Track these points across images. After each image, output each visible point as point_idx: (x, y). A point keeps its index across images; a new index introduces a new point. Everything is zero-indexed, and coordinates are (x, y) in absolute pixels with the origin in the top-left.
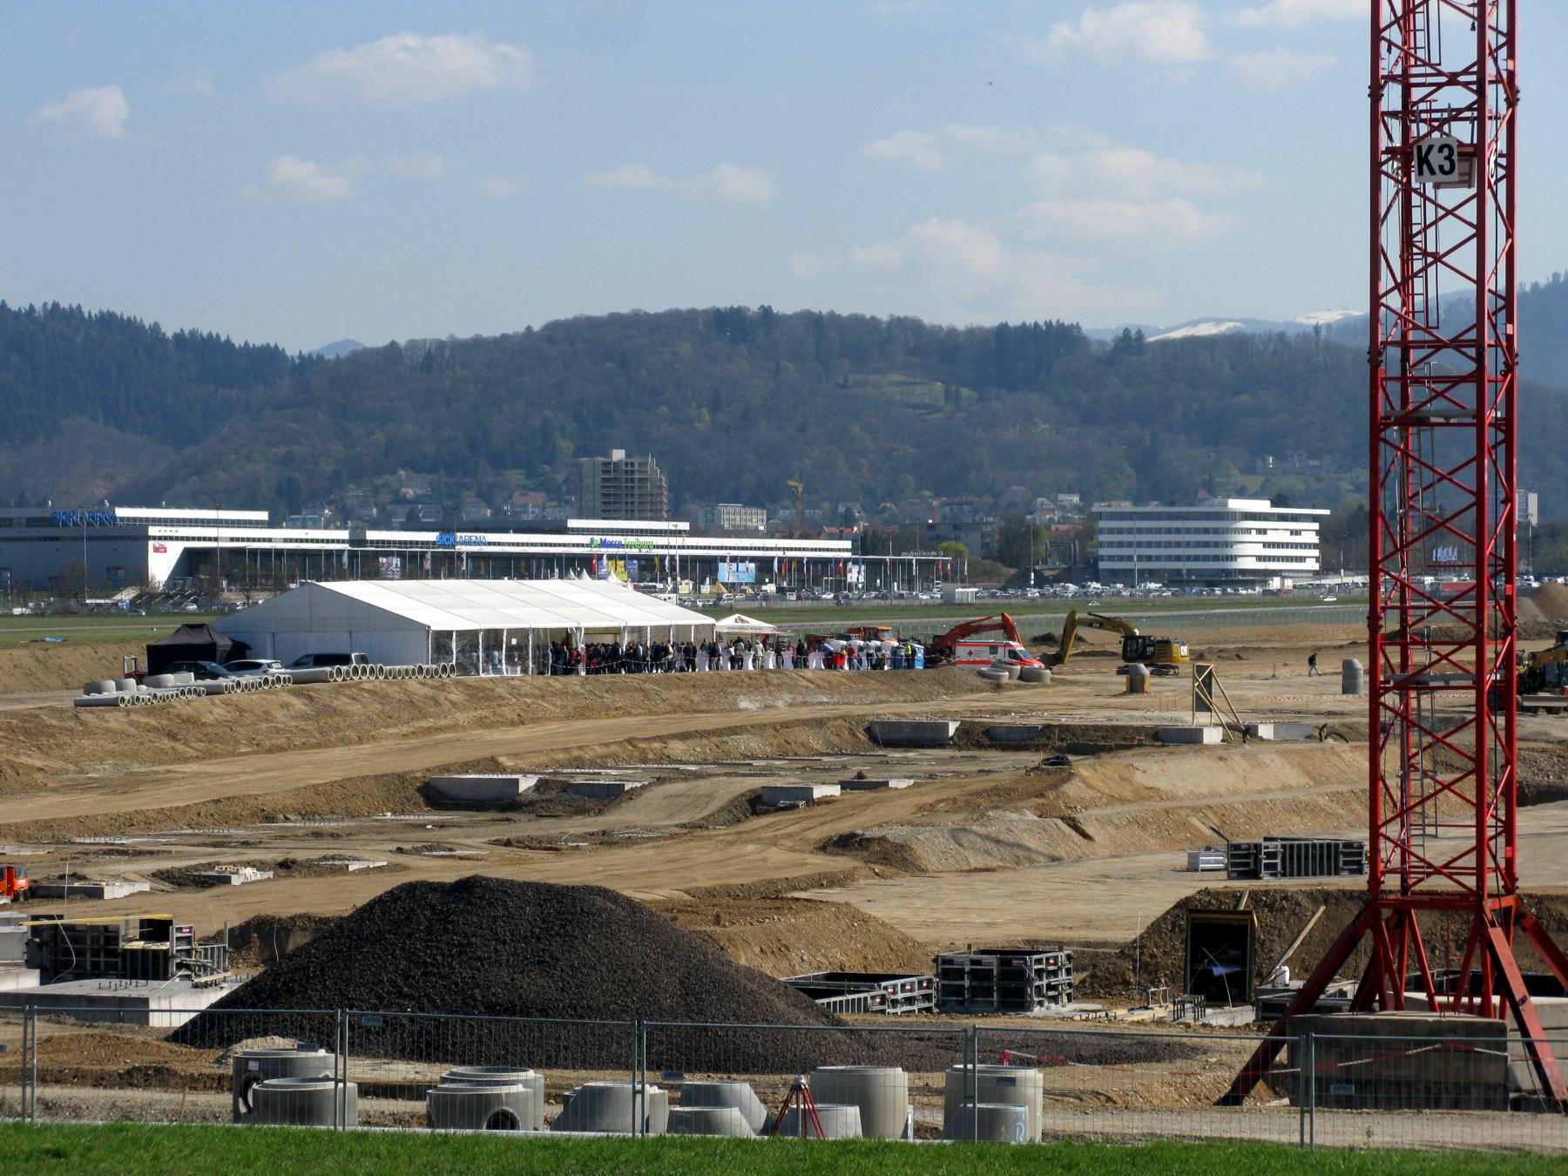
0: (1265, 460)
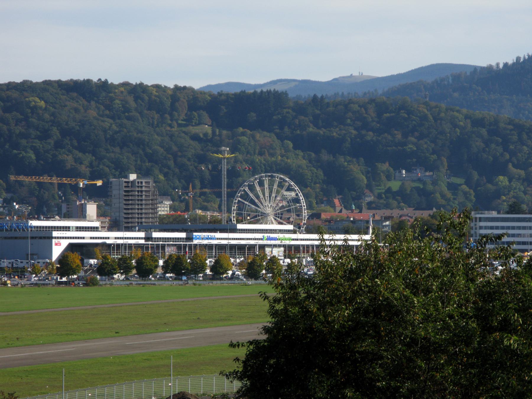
0: (400, 172)
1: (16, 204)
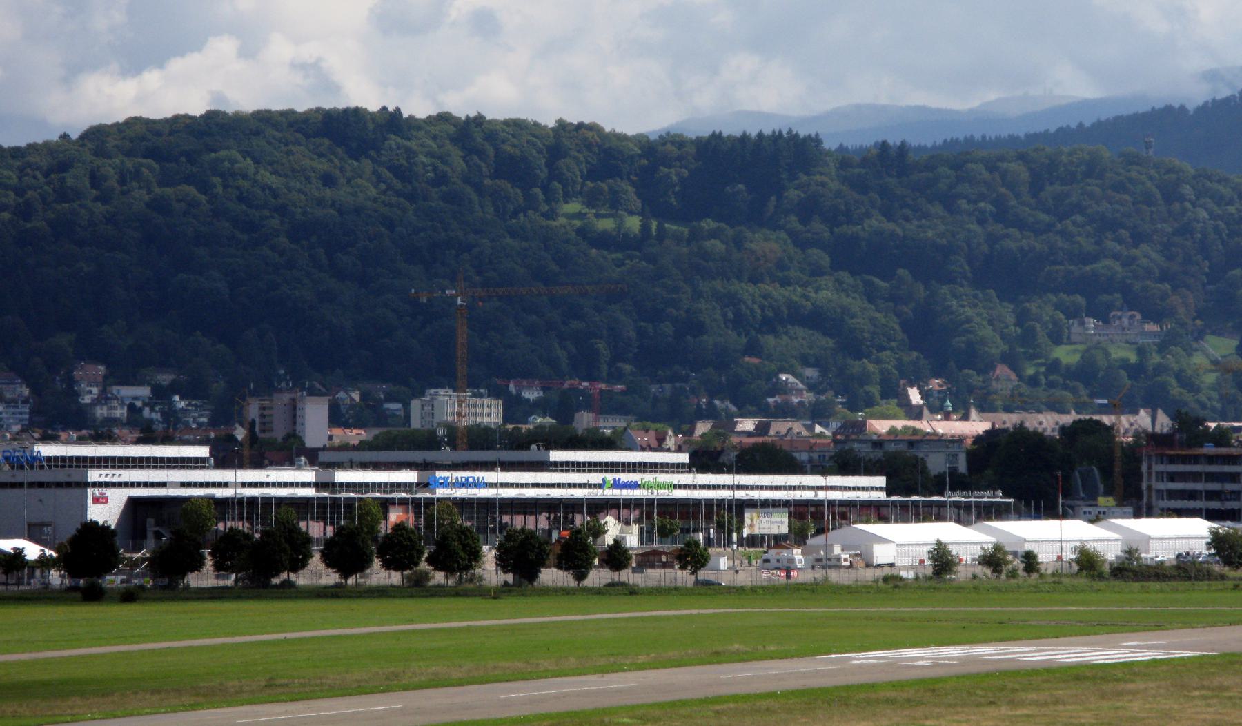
1: (181, 399)
